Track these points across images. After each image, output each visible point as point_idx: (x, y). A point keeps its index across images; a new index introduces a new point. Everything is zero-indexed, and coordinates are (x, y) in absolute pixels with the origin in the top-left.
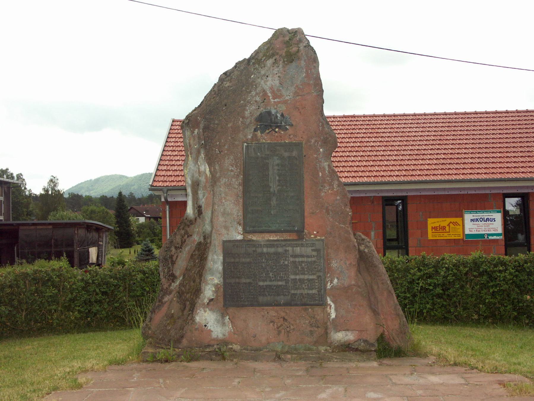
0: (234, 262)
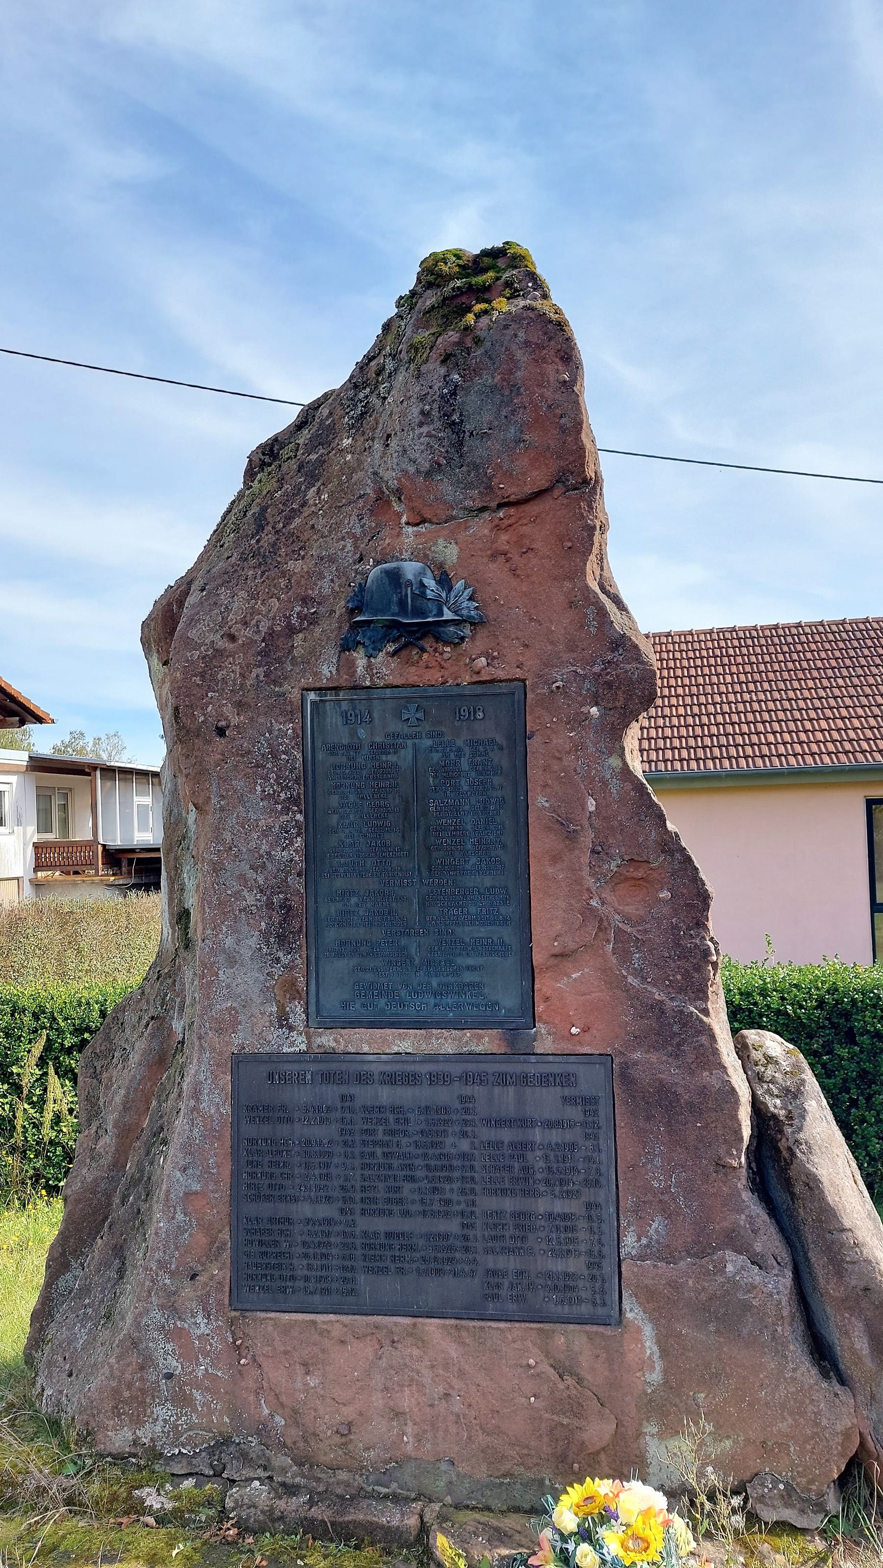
0: (738, 1191)
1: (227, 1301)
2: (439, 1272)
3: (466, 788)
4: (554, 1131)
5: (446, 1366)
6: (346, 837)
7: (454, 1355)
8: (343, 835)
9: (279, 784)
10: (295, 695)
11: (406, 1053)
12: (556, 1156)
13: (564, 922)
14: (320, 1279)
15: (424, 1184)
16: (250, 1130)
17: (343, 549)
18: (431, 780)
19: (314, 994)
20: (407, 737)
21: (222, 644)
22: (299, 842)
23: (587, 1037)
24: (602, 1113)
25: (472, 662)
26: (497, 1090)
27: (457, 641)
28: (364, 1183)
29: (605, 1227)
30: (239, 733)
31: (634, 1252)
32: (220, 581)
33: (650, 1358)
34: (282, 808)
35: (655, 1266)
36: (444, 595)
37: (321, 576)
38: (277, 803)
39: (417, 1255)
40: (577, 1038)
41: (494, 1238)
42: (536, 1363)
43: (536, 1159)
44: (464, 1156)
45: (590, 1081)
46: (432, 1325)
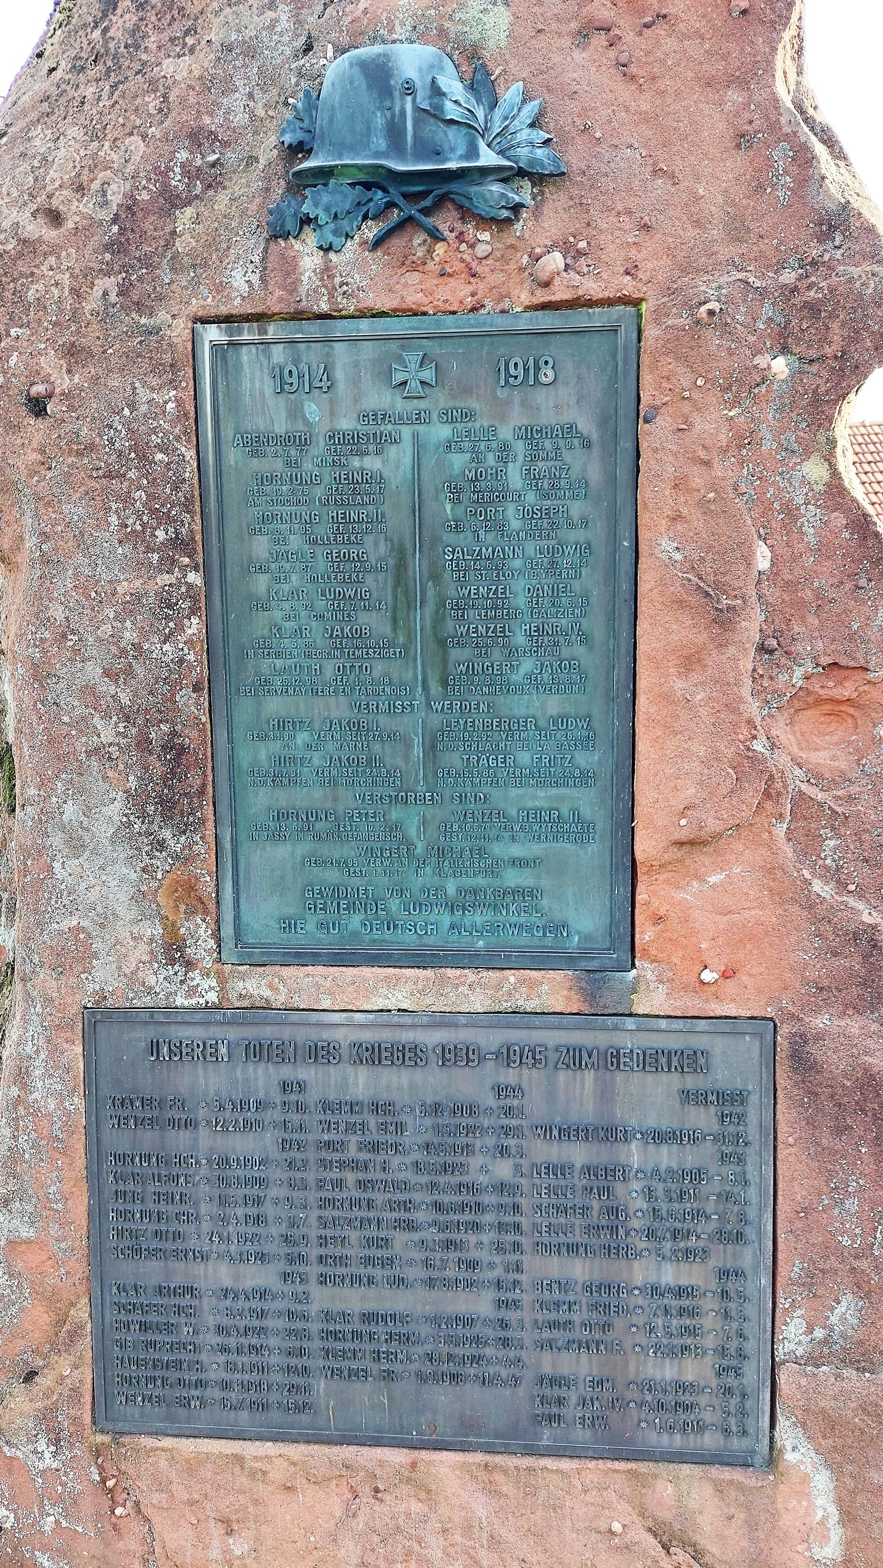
1: (87, 1418)
2: (455, 1378)
3: (515, 524)
4: (664, 1149)
5: (468, 1529)
6: (288, 618)
7: (482, 1513)
8: (278, 615)
9: (153, 512)
10: (179, 331)
11: (399, 1010)
12: (667, 1191)
13: (700, 783)
14: (246, 1387)
15: (431, 1234)
16: (120, 1140)
17: (272, 27)
18: (448, 507)
19: (231, 905)
20: (401, 420)
21: (37, 229)
22: (194, 626)
23: (730, 987)
24: (752, 1117)
25: (535, 255)
26: (563, 1076)
27: (505, 213)
28: (323, 1232)
29: (750, 1310)
30: (71, 408)
31: (800, 1352)
32: (34, 115)
33: (823, 1522)
34: (161, 559)
35: (837, 1376)
36: (480, 113)
37: (228, 89)
38: (149, 549)
39: (420, 1350)
40: (713, 988)
41: (554, 1325)
42: (624, 1526)
43: (632, 1195)
44: (501, 1187)
45: (734, 1063)
46: (444, 1464)
